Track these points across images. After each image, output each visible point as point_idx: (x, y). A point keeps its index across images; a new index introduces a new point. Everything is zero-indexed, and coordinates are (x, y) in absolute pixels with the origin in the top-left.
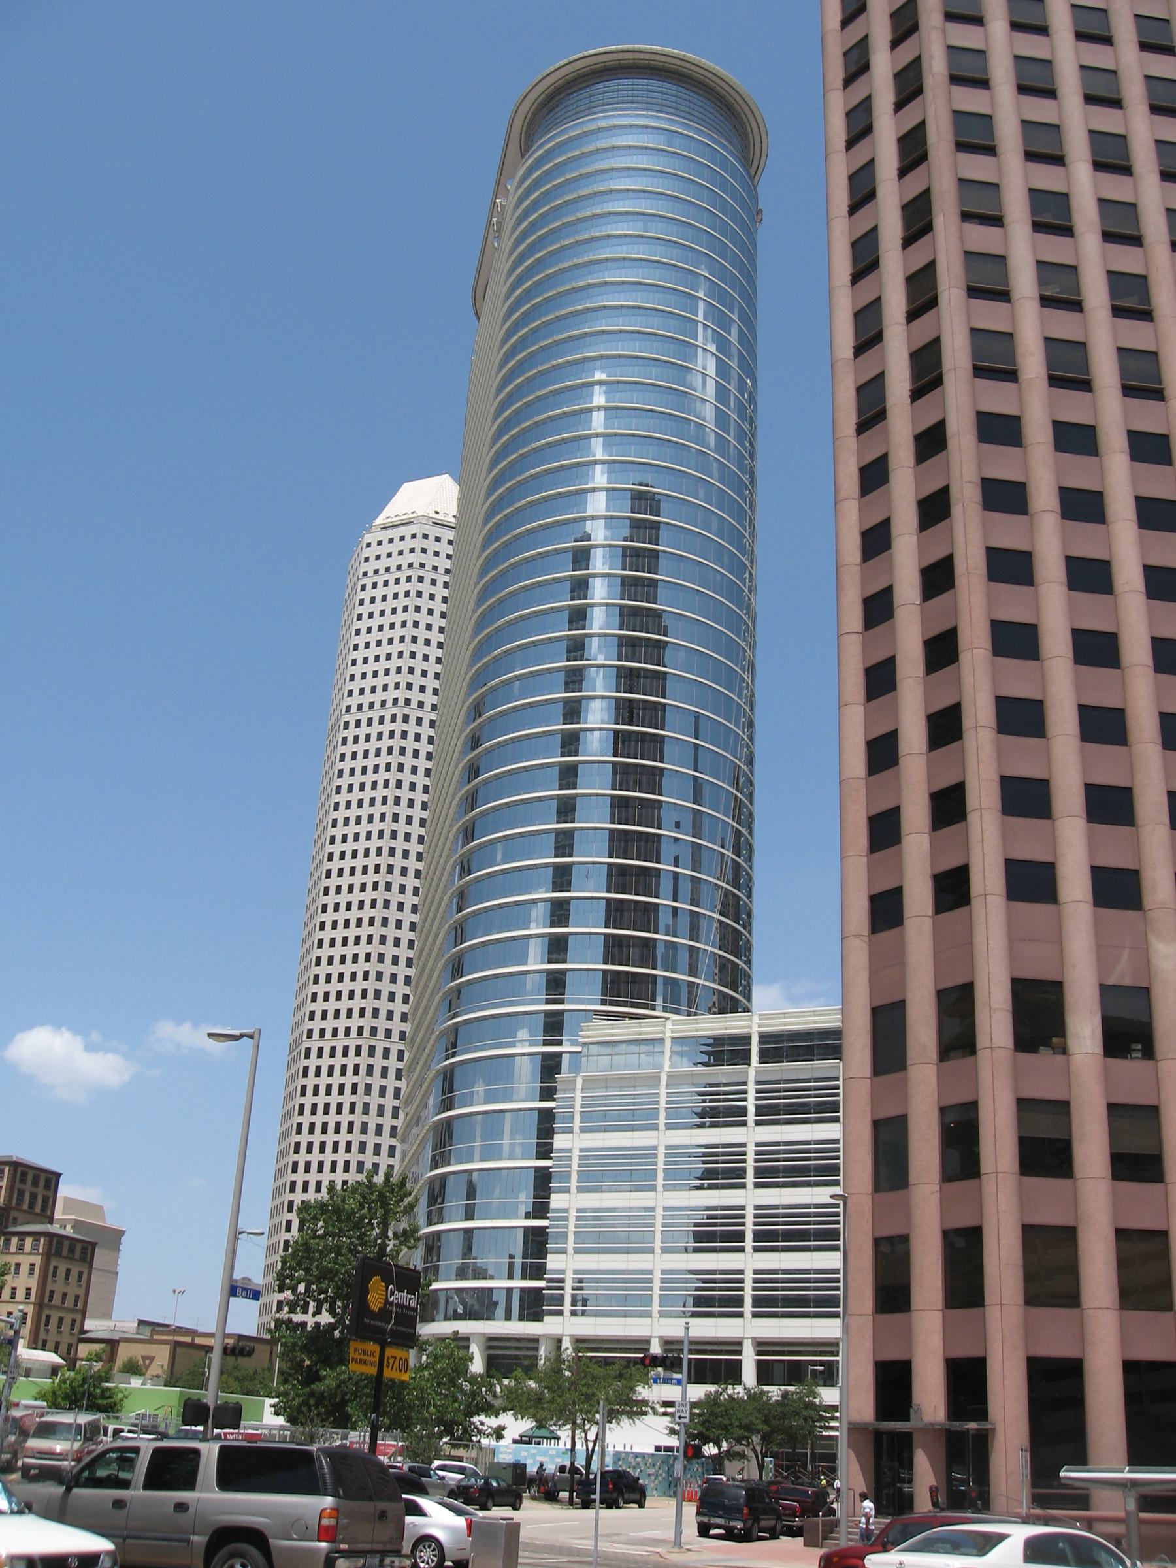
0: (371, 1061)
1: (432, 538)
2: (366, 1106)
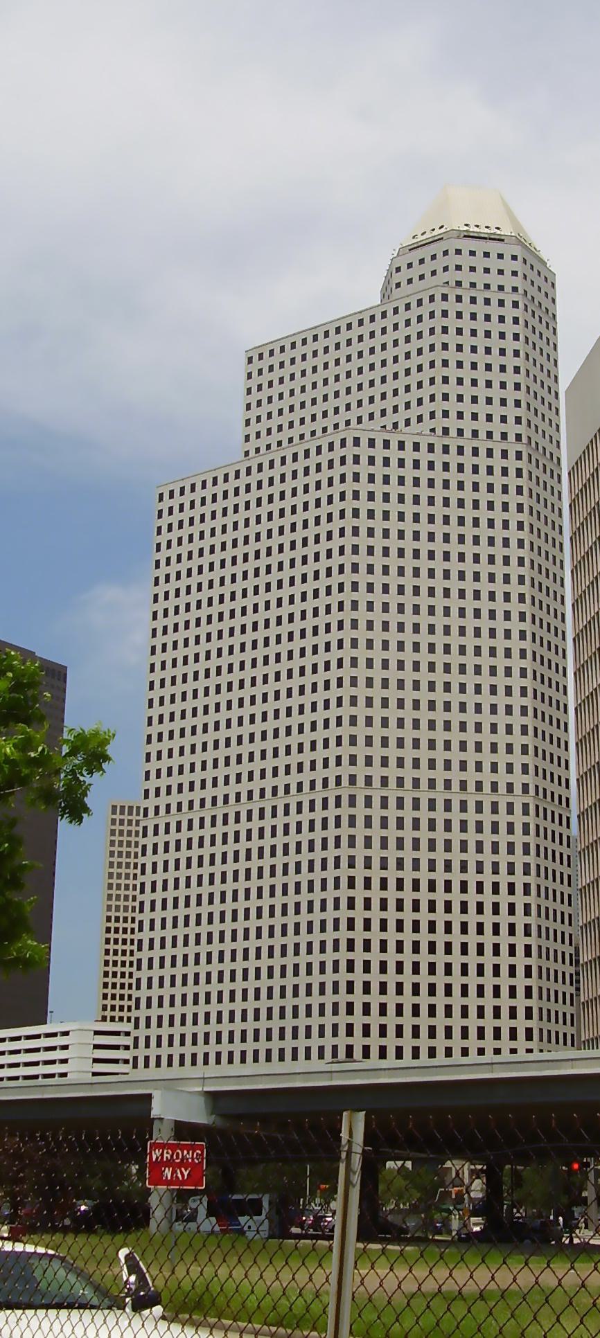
0: (352, 811)
1: (465, 252)
2: (352, 839)
